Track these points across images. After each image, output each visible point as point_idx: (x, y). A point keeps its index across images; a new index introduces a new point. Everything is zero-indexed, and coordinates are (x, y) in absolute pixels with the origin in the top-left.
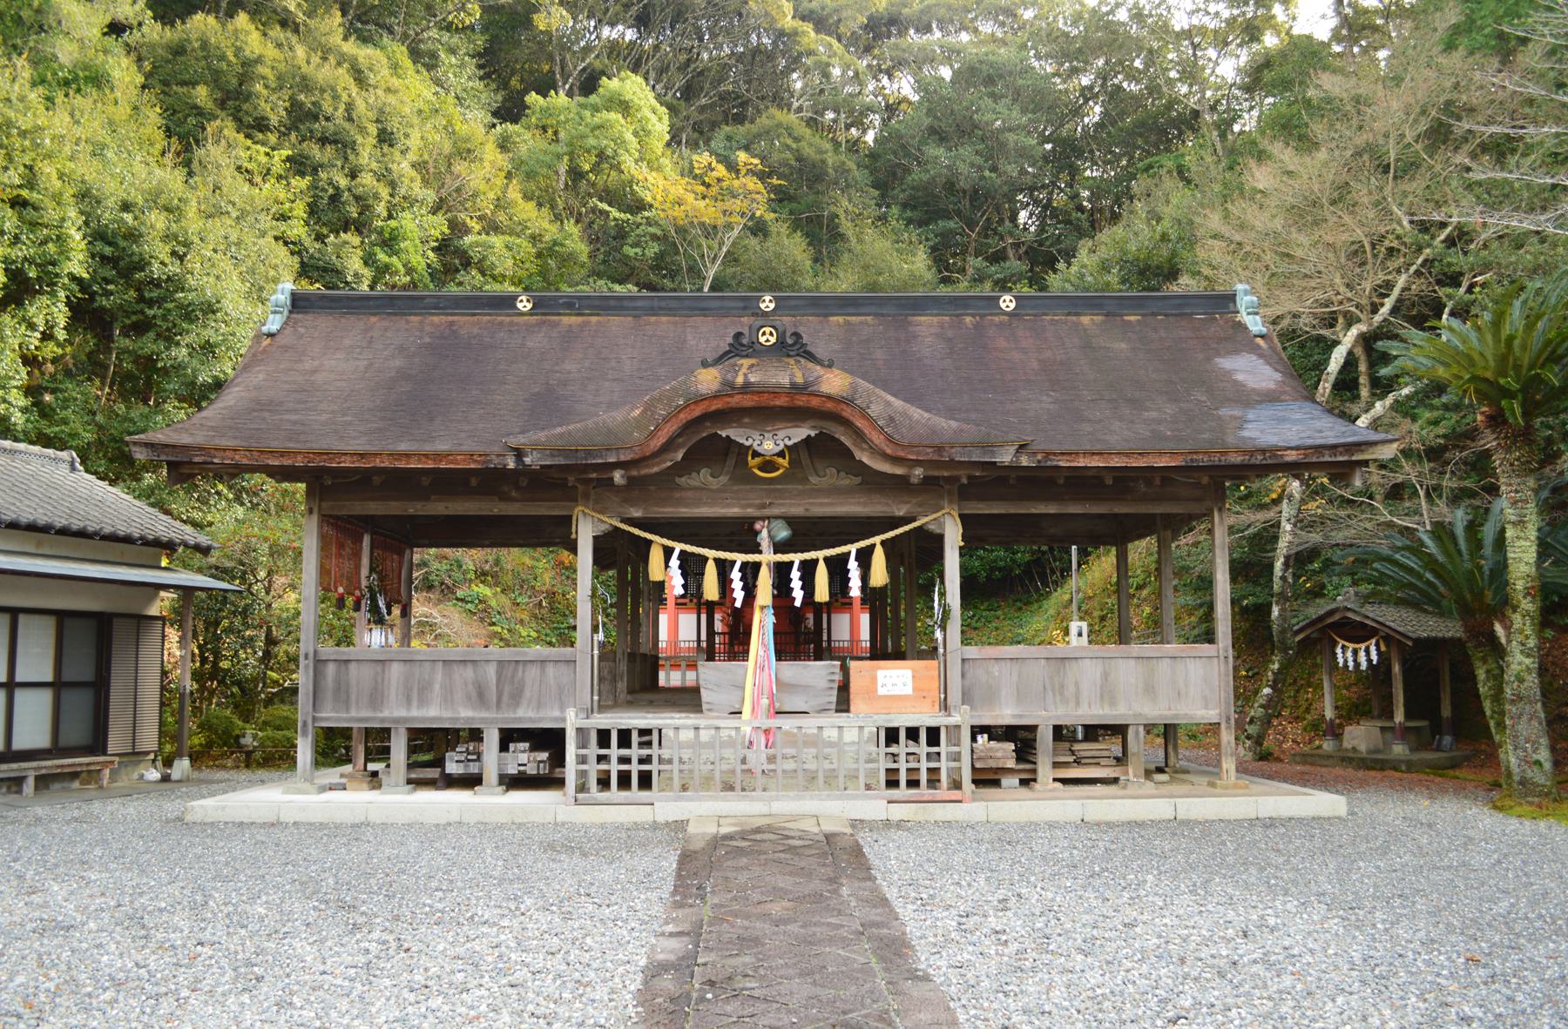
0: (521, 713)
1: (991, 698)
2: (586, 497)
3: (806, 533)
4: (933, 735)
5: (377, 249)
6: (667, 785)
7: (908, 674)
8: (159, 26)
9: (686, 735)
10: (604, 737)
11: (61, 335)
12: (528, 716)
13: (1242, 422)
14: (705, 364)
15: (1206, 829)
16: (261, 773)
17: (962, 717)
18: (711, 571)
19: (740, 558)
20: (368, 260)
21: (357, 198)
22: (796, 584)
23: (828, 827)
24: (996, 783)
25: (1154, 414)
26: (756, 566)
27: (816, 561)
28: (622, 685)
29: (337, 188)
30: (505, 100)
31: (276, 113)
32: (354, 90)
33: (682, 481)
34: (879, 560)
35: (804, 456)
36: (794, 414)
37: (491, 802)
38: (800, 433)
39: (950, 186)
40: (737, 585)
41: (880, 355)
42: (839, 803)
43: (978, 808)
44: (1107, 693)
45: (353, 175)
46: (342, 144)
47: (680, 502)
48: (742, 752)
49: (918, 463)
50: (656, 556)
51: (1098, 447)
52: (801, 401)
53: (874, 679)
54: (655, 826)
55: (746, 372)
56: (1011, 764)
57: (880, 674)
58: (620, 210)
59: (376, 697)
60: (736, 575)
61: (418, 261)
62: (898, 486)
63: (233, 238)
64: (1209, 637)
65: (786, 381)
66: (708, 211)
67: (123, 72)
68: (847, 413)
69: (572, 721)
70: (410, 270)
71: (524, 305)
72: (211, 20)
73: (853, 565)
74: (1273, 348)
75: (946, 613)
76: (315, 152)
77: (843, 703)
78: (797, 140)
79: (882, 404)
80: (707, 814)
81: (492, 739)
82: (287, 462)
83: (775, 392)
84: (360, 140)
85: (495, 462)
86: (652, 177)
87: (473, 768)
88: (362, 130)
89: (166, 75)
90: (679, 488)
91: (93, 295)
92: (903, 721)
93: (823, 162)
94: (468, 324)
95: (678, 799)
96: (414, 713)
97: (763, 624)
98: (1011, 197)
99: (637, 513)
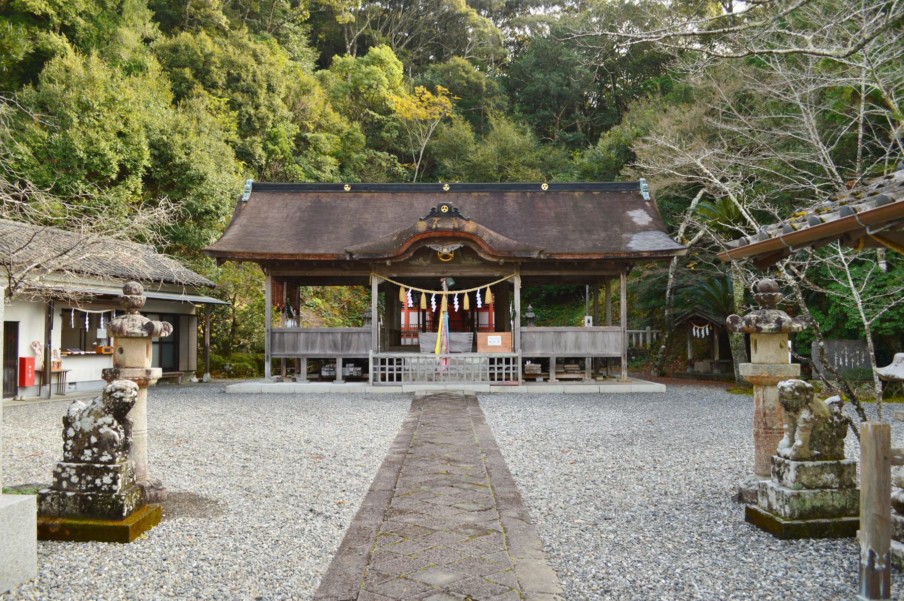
0: (351, 352)
1: (532, 346)
2: (375, 269)
3: (460, 283)
4: (507, 361)
5: (268, 142)
6: (407, 379)
7: (500, 337)
8: (164, 38)
9: (414, 361)
10: (383, 361)
11: (140, 192)
12: (353, 353)
13: (630, 239)
14: (421, 220)
15: (617, 396)
16: (236, 380)
17: (519, 354)
18: (423, 299)
19: (434, 293)
20: (265, 148)
21: (259, 119)
22: (456, 303)
23: (466, 393)
24: (534, 380)
25: (596, 237)
26: (441, 296)
27: (464, 294)
28: (387, 343)
29: (250, 115)
30: (321, 55)
31: (221, 81)
32: (255, 66)
33: (412, 262)
34: (488, 293)
35: (460, 253)
36: (455, 239)
37: (339, 386)
38: (457, 246)
39: (547, 93)
40: (433, 303)
41: (491, 210)
42: (472, 386)
43: (524, 388)
44: (577, 345)
45: (257, 108)
46: (251, 93)
47: (411, 271)
48: (435, 367)
49: (502, 257)
50: (402, 291)
51: (571, 251)
52: (457, 234)
53: (486, 340)
54: (403, 394)
55: (437, 224)
56: (539, 372)
57: (489, 337)
58: (380, 114)
59: (295, 347)
60: (433, 299)
61: (286, 147)
62: (495, 265)
63: (208, 143)
64: (618, 324)
65: (451, 227)
66: (422, 113)
67: (152, 63)
68: (475, 238)
69: (371, 355)
70: (283, 152)
71: (347, 188)
72: (189, 35)
73: (478, 295)
74: (652, 207)
75: (515, 313)
76: (239, 97)
77: (475, 348)
78: (467, 73)
79: (489, 234)
80: (422, 388)
81: (340, 362)
82: (263, 257)
83: (448, 231)
84: (259, 91)
85: (342, 258)
86: (396, 98)
87: (332, 374)
88: (260, 86)
89: (172, 61)
90: (411, 265)
91: (151, 173)
92: (496, 355)
93: (481, 83)
94: (326, 198)
95: (411, 384)
96: (310, 352)
97: (444, 318)
98: (573, 101)
99: (395, 275)
